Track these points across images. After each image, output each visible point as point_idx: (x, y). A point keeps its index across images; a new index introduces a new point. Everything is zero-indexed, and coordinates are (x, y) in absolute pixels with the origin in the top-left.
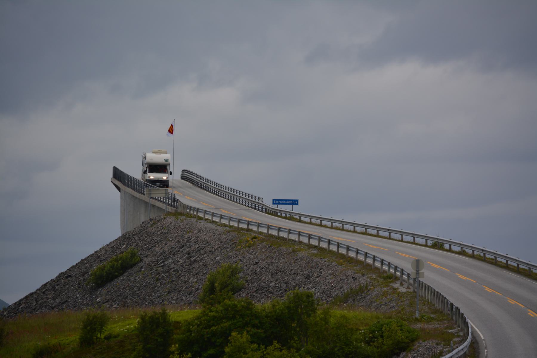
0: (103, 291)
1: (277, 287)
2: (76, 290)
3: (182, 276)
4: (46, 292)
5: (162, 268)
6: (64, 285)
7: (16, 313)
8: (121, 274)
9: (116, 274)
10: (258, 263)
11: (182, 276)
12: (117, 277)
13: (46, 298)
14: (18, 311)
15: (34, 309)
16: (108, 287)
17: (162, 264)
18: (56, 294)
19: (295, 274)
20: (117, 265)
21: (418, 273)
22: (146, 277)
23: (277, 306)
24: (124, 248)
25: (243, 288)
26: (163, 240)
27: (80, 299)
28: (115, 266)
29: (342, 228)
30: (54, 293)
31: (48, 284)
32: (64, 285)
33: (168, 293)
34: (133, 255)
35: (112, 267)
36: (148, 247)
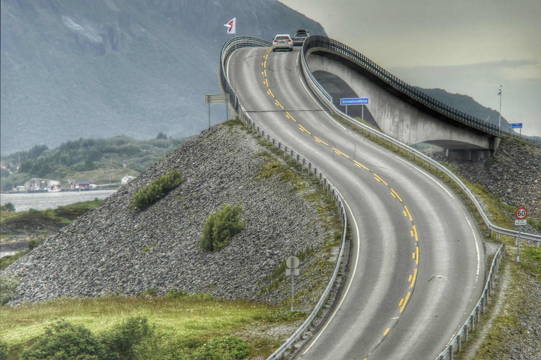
0: (142, 215)
1: (266, 232)
2: (125, 211)
3: (207, 206)
4: (103, 210)
5: (196, 193)
6: (119, 203)
7: (73, 233)
8: (163, 197)
9: (158, 196)
10: (265, 199)
11: (207, 206)
12: (158, 200)
13: (101, 217)
14: (74, 231)
15: (88, 230)
16: (151, 209)
17: (198, 189)
18: (110, 214)
19: (284, 218)
20: (158, 188)
21: (53, 204)
22: (180, 202)
23: (289, 268)
24: (178, 162)
25: (243, 230)
26: (209, 157)
27: (124, 223)
28: (156, 189)
29: (441, 146)
30: (108, 212)
31: (108, 199)
32: (119, 203)
33: (190, 226)
34: (176, 176)
35: (154, 190)
36: (196, 164)
